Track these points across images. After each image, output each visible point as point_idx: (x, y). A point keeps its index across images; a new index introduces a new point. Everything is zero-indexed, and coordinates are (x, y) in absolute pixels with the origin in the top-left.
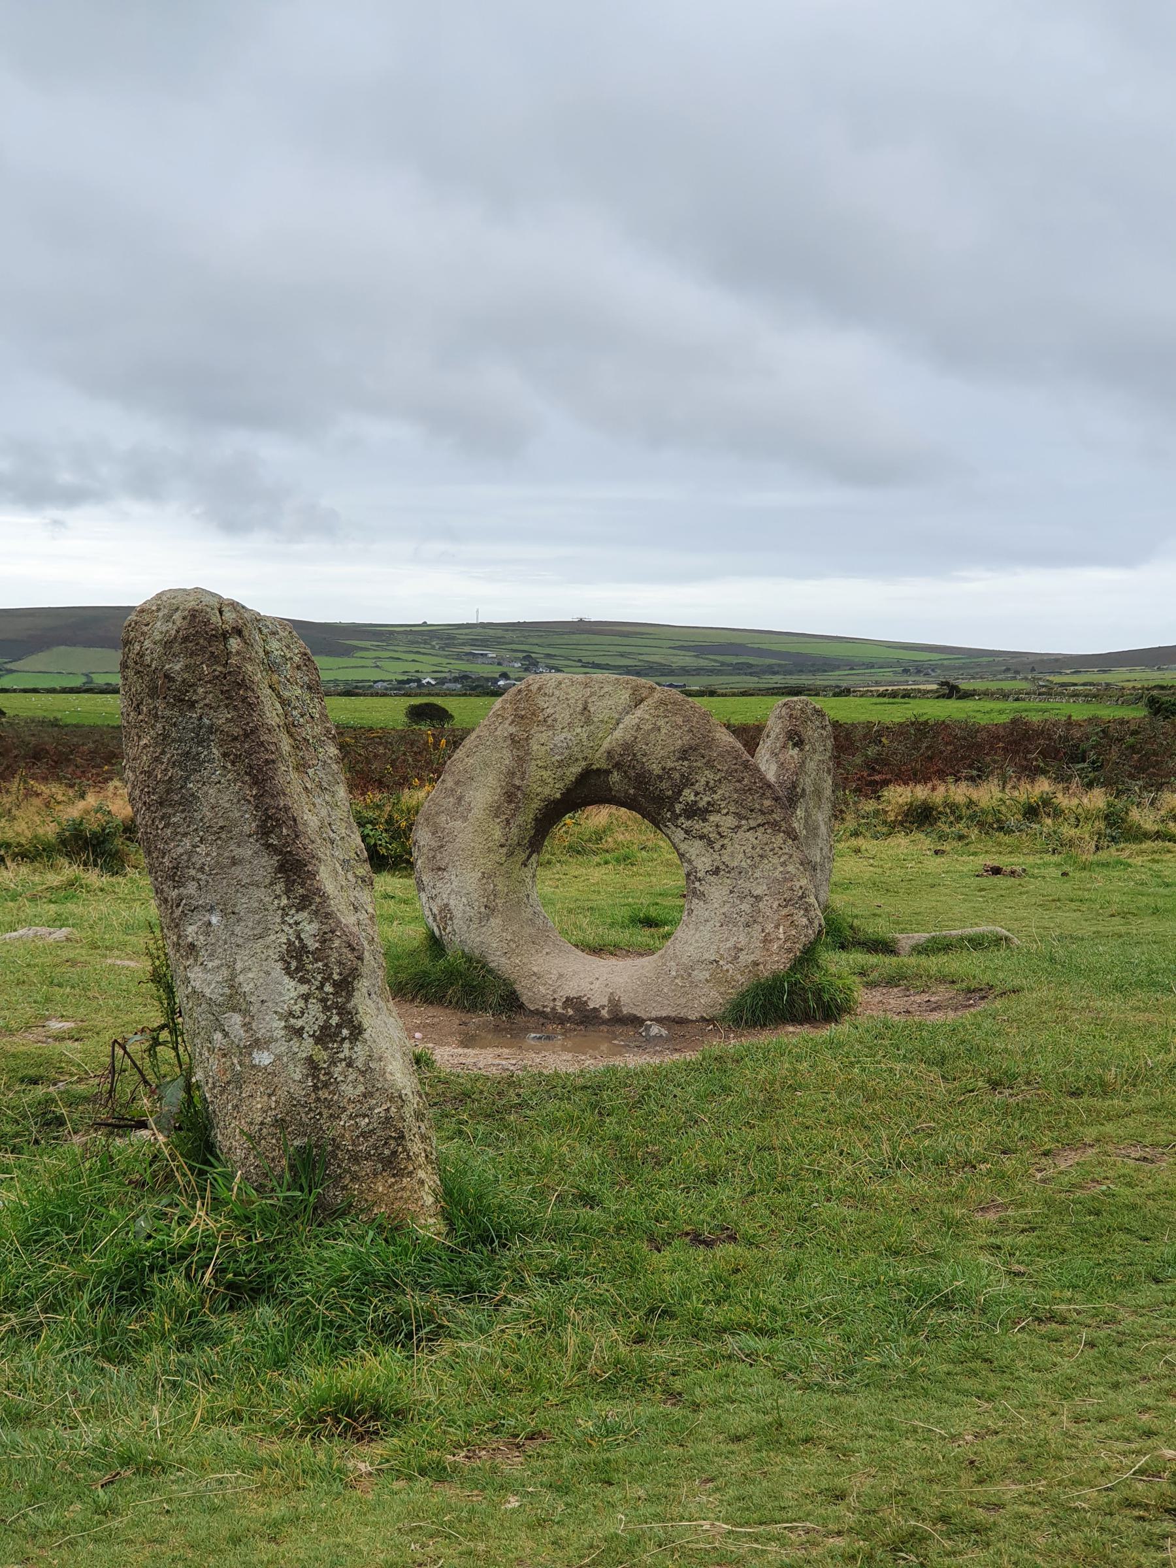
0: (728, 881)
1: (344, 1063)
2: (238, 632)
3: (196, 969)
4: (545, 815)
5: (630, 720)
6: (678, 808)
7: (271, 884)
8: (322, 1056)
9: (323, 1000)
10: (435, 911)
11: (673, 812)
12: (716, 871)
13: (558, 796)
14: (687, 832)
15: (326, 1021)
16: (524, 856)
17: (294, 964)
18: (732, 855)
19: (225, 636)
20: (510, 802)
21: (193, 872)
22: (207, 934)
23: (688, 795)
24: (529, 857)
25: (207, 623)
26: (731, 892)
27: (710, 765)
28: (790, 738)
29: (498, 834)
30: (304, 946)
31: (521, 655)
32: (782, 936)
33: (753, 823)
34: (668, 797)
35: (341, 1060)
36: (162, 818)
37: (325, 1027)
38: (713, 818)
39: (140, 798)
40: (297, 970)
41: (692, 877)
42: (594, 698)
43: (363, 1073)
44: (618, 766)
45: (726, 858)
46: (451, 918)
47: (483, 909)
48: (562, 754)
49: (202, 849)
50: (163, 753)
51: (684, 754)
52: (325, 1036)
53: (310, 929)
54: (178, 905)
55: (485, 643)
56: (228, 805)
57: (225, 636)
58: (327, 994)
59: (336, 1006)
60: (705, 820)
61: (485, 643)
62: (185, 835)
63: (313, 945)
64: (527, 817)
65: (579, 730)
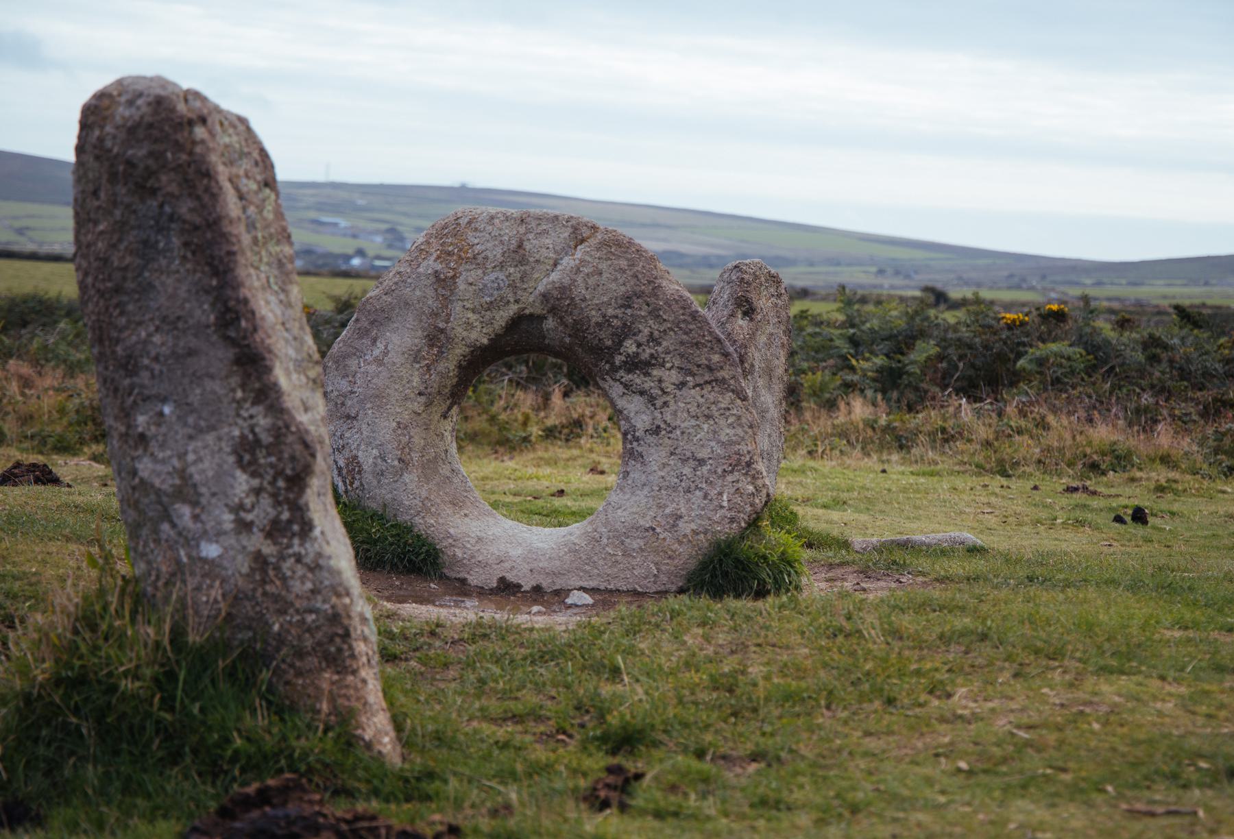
0: (670, 442)
1: (292, 560)
2: (203, 120)
3: (145, 460)
4: (470, 363)
5: (567, 262)
6: (618, 360)
7: (227, 377)
8: (268, 549)
9: (274, 496)
10: (341, 463)
11: (613, 364)
12: (656, 431)
13: (485, 341)
14: (626, 386)
16: (444, 407)
17: (247, 457)
18: (675, 413)
19: (191, 123)
20: (431, 346)
21: (146, 361)
22: (159, 425)
23: (630, 346)
24: (449, 408)
25: (173, 110)
26: (672, 454)
27: (655, 314)
28: (739, 306)
29: (416, 381)
31: (384, 226)
32: (725, 504)
33: (699, 380)
34: (608, 348)
35: (290, 556)
36: (117, 306)
37: (275, 522)
38: (656, 372)
39: (93, 285)
40: (250, 463)
41: (629, 437)
42: (531, 236)
43: (311, 570)
44: (553, 310)
45: (668, 418)
46: (359, 472)
47: (396, 463)
48: (492, 295)
49: (157, 339)
50: (120, 240)
51: (627, 302)
52: (275, 530)
54: (130, 394)
55: (337, 208)
57: (191, 123)
58: (279, 489)
59: (287, 500)
60: (647, 374)
61: (337, 208)
62: (140, 324)
63: (266, 438)
64: (449, 365)
65: (512, 270)
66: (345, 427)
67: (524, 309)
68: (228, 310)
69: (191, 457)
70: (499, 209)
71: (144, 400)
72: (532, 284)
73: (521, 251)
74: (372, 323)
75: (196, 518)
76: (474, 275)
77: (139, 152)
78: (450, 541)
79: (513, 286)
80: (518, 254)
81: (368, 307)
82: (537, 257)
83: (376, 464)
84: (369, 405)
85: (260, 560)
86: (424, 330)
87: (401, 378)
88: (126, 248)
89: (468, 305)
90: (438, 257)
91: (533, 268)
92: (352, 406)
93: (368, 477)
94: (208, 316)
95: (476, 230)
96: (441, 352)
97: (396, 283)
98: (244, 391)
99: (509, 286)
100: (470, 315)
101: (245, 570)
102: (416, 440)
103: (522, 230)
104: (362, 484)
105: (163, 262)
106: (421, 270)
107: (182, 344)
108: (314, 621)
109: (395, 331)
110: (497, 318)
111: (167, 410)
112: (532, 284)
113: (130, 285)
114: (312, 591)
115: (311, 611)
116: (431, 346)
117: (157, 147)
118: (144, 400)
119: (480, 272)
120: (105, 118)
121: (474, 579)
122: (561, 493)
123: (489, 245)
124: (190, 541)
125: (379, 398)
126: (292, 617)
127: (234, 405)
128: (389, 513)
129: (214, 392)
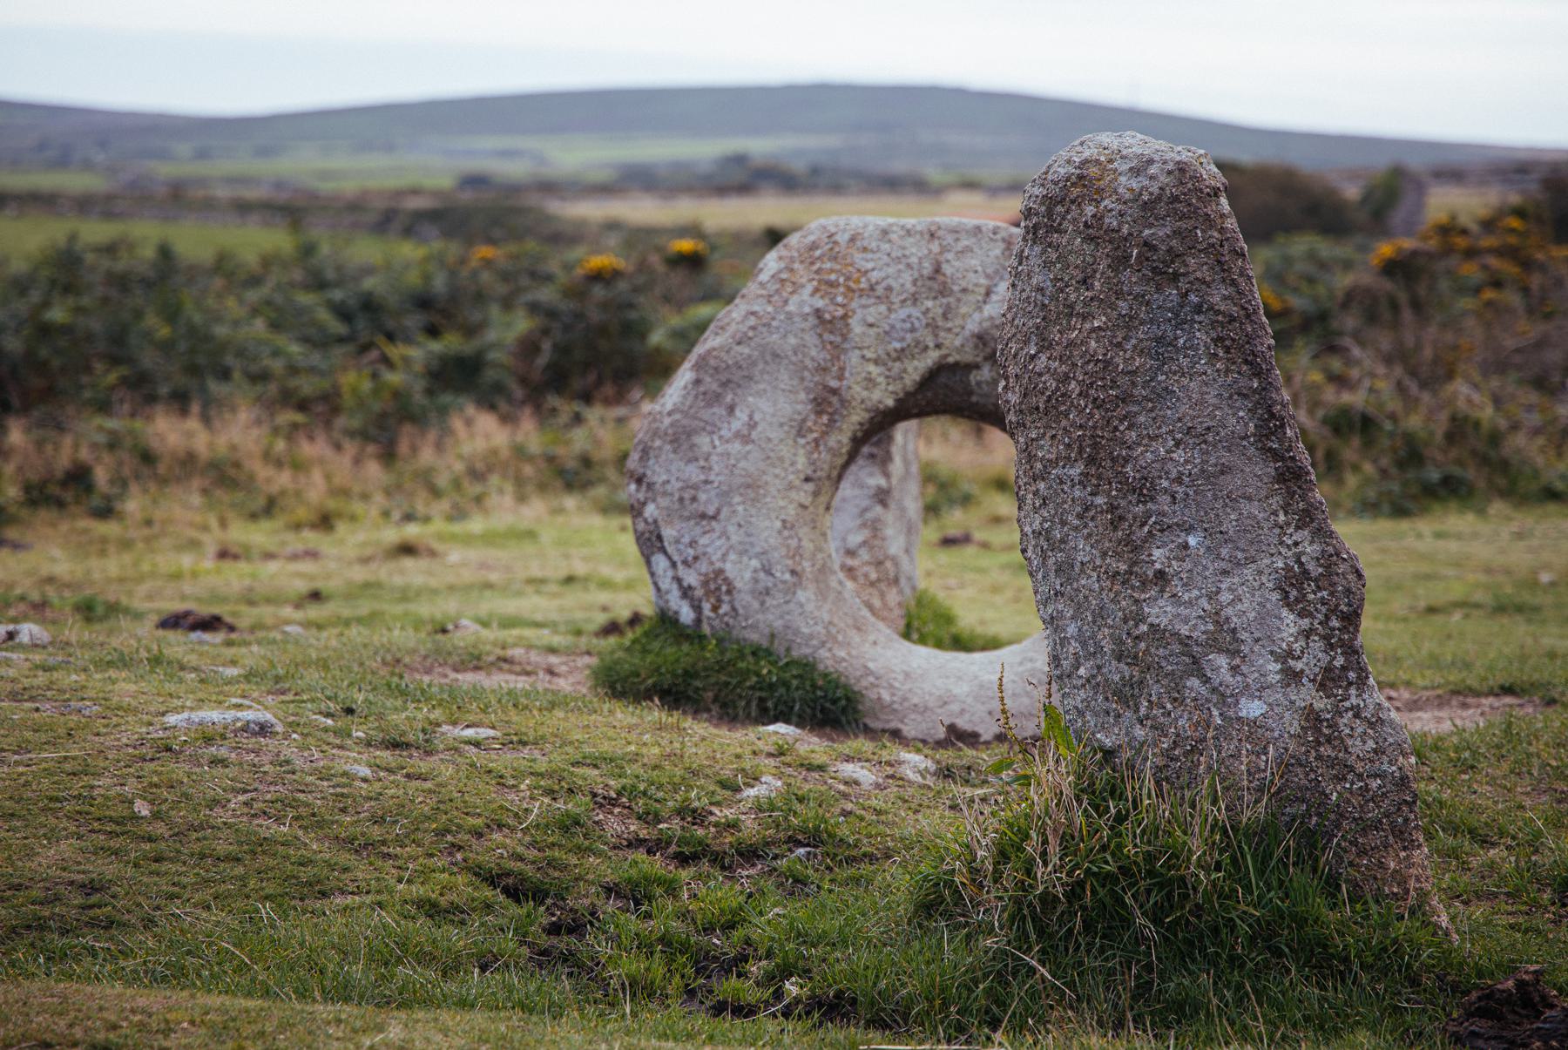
1: (1350, 714)
15: (1330, 663)
20: (819, 413)
21: (1165, 484)
29: (801, 461)
30: (1306, 572)
35: (1347, 710)
37: (1328, 669)
40: (1297, 601)
42: (950, 256)
43: (1371, 725)
46: (729, 592)
47: (787, 576)
48: (903, 339)
49: (1180, 455)
52: (1328, 680)
53: (1311, 549)
54: (1143, 525)
56: (1215, 401)
58: (1333, 629)
63: (1315, 570)
65: (929, 304)
66: (698, 530)
67: (947, 356)
68: (1272, 416)
69: (1225, 597)
70: (891, 220)
71: (1162, 531)
72: (958, 322)
73: (941, 278)
74: (724, 384)
75: (1235, 670)
76: (875, 312)
77: (1156, 232)
78: (871, 679)
79: (933, 327)
80: (936, 281)
81: (712, 362)
82: (963, 284)
83: (756, 581)
84: (737, 499)
85: (1312, 718)
86: (808, 391)
87: (781, 459)
88: (1135, 347)
89: (869, 355)
90: (816, 290)
91: (959, 300)
92: (707, 500)
93: (744, 599)
94: (1246, 424)
95: (865, 249)
96: (832, 421)
97: (753, 328)
98: (1286, 513)
99: (928, 325)
100: (872, 368)
101: (1295, 728)
102: (807, 544)
103: (935, 247)
104: (734, 609)
105: (1184, 362)
106: (791, 308)
107: (1213, 461)
108: (1380, 787)
109: (759, 394)
110: (910, 370)
111: (1192, 541)
112: (958, 322)
113: (1138, 392)
114: (1375, 751)
115: (1376, 776)
116: (819, 413)
117: (1183, 225)
118: (1162, 531)
119: (883, 308)
120: (1100, 191)
121: (909, 730)
122: (316, 596)
123: (891, 270)
124: (1224, 698)
125: (752, 488)
126: (1352, 783)
127: (1277, 531)
128: (778, 647)
129: (1251, 516)
